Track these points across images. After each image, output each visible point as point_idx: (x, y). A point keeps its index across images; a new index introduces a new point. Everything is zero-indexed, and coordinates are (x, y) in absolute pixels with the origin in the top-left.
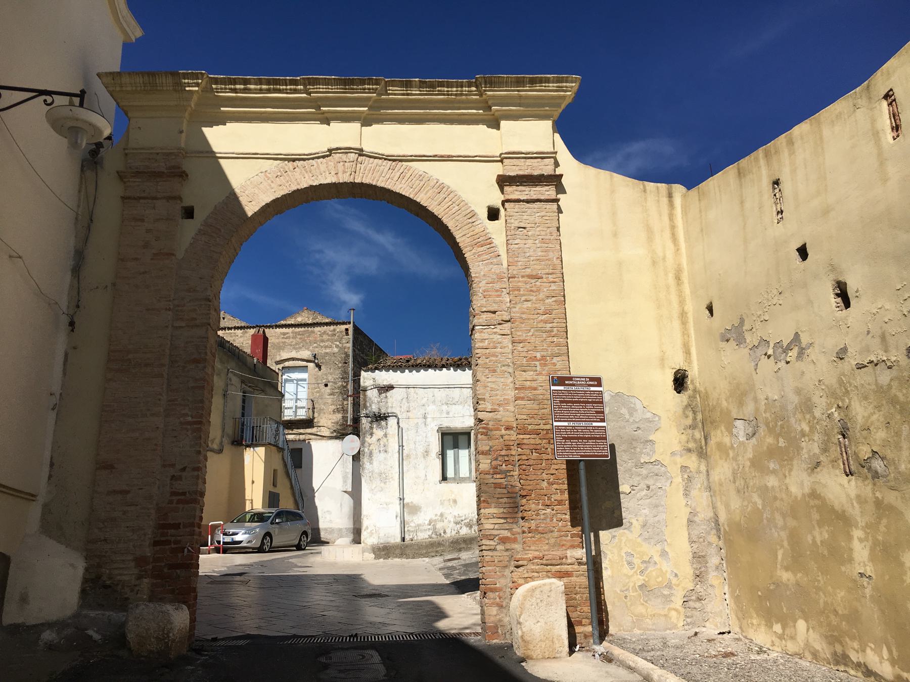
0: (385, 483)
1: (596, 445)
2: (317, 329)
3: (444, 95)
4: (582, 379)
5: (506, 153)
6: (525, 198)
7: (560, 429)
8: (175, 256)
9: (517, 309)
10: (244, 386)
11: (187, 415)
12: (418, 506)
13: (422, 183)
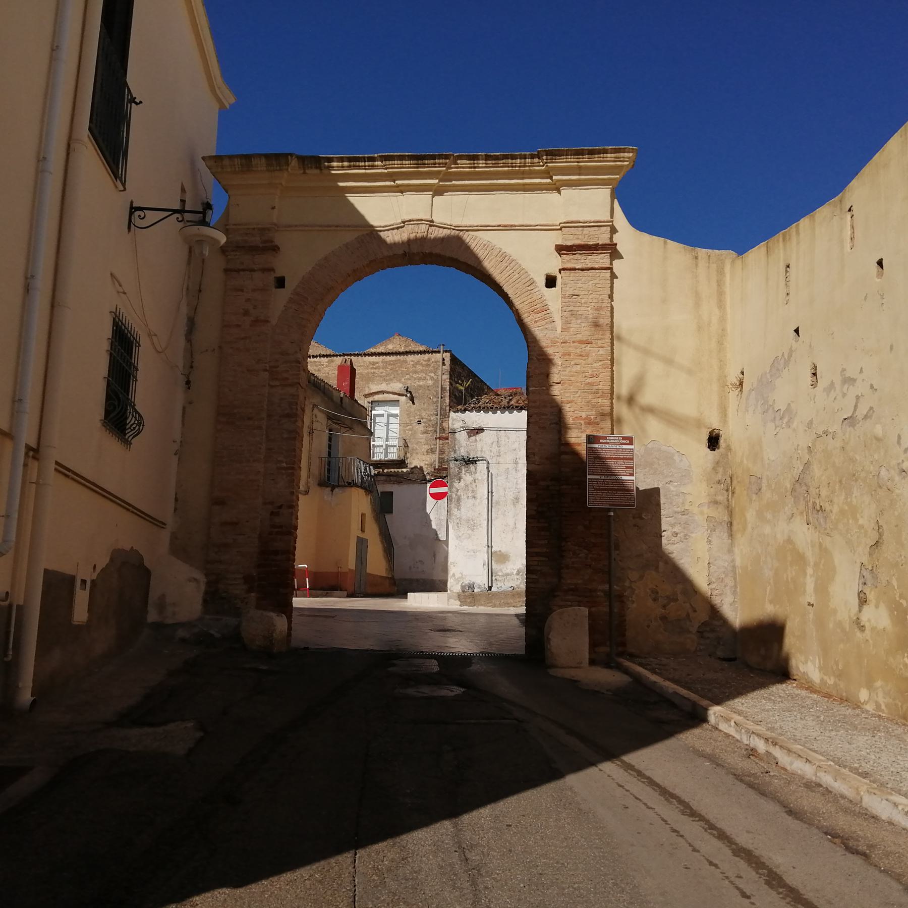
0: (473, 530)
1: (624, 496)
2: (410, 358)
3: (509, 167)
4: (616, 438)
5: (564, 223)
6: (580, 266)
7: (593, 482)
8: (270, 322)
9: (566, 373)
10: (330, 422)
11: (282, 462)
12: (506, 555)
13: (486, 252)
